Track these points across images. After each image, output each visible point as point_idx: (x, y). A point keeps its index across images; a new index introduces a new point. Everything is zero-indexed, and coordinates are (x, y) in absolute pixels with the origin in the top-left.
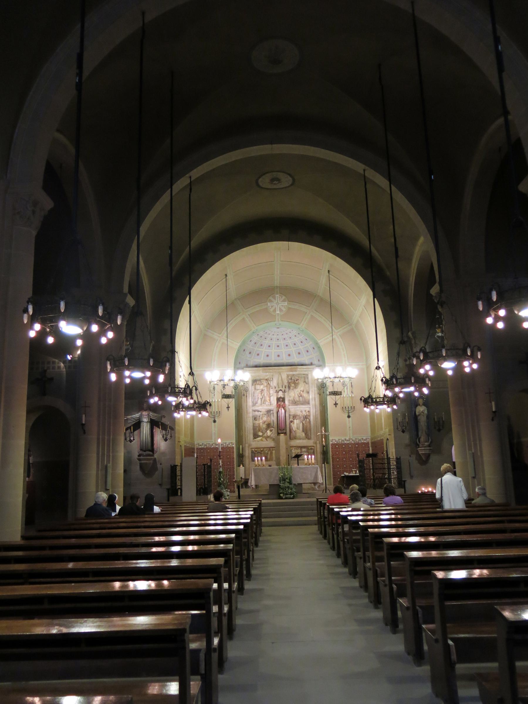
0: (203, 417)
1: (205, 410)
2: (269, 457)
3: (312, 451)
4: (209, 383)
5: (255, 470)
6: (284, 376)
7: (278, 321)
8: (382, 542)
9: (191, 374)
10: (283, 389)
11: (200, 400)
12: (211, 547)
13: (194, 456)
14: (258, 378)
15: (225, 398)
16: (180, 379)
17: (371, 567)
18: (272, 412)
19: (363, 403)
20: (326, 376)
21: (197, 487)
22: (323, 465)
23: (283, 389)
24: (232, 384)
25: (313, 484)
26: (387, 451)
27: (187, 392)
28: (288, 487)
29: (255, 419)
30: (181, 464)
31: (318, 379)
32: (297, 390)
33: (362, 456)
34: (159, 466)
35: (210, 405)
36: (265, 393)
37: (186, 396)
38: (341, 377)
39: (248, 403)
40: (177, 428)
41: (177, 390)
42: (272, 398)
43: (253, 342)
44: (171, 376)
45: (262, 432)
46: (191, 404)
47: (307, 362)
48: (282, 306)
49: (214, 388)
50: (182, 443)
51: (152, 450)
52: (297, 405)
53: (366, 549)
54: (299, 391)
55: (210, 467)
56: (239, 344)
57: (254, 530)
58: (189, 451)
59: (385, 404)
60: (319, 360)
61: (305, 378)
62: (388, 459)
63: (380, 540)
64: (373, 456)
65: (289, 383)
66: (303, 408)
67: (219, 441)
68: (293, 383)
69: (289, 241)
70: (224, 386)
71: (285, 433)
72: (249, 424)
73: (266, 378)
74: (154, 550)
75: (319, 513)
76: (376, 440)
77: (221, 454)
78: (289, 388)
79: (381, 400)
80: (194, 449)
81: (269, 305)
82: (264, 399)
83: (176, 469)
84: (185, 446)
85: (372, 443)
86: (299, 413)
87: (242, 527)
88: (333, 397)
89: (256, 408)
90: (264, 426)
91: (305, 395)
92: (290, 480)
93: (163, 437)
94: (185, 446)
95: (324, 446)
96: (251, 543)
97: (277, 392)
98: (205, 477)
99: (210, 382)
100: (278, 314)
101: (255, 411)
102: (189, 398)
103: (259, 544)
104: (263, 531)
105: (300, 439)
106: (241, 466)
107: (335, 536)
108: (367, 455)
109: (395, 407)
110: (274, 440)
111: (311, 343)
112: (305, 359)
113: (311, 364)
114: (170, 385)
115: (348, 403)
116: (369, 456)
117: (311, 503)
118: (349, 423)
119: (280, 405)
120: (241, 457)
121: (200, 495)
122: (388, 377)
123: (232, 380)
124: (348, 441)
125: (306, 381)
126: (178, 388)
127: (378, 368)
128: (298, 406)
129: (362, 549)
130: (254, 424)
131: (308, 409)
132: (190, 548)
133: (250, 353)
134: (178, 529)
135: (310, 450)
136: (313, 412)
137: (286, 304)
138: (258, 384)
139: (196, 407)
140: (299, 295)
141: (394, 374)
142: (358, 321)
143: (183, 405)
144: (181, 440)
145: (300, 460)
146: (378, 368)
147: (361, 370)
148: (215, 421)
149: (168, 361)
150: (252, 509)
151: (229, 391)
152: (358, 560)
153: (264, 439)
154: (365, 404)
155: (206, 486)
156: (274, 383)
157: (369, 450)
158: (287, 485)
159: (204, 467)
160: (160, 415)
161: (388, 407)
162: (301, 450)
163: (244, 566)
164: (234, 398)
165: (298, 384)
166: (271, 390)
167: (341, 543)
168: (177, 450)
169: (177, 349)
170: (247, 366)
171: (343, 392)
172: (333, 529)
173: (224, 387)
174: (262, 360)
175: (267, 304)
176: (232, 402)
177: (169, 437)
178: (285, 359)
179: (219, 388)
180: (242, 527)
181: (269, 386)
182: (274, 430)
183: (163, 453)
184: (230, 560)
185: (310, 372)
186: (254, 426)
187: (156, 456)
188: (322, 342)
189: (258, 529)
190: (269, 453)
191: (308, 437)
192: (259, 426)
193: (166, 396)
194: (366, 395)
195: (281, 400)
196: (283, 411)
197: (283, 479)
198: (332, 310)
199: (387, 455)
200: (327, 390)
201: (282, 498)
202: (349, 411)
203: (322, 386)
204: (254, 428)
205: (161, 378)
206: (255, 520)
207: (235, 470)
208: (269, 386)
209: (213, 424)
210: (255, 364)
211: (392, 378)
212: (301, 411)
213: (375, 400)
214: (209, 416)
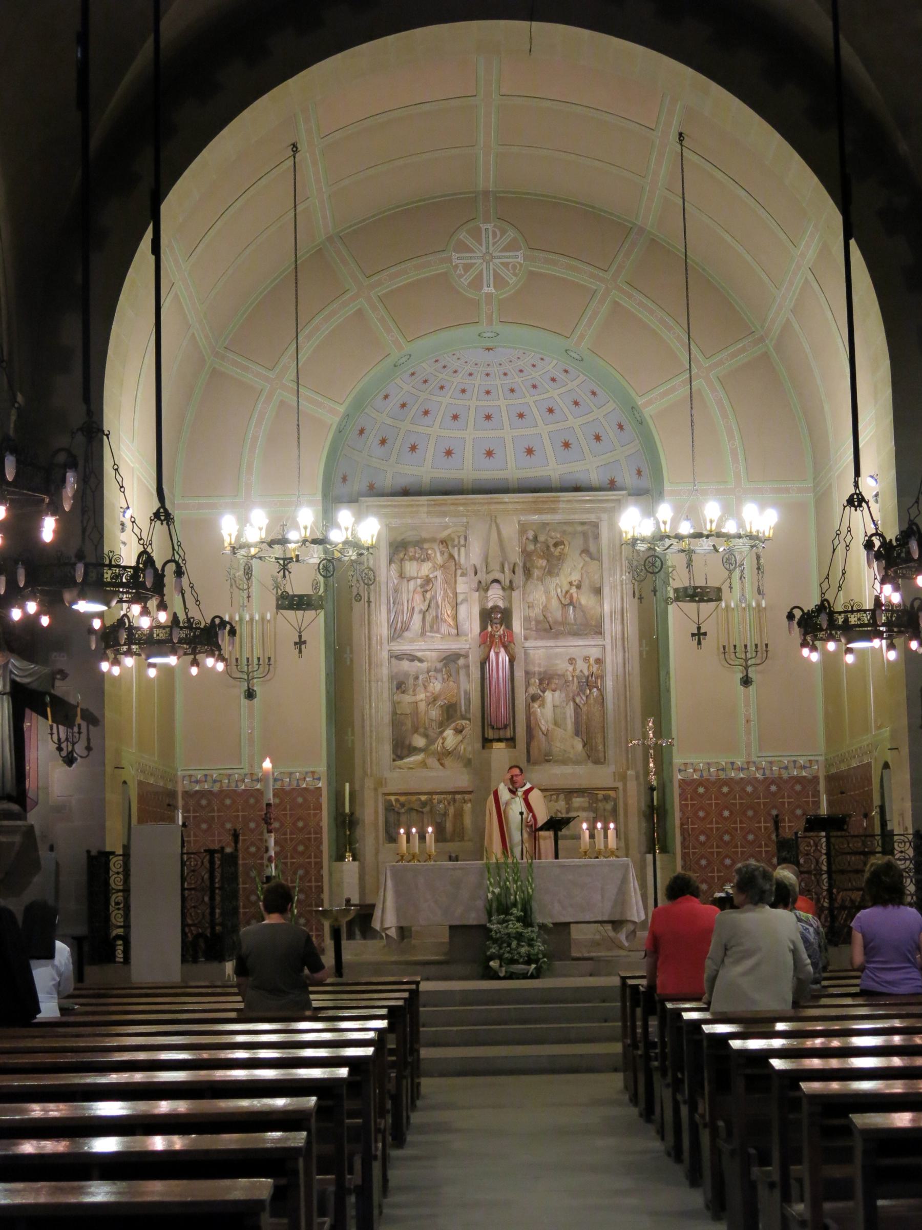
0: (206, 673)
1: (214, 649)
2: (449, 826)
3: (609, 806)
4: (228, 550)
5: (398, 876)
6: (510, 529)
7: (490, 322)
8: (848, 1130)
9: (163, 515)
10: (505, 578)
11: (194, 613)
12: (230, 1141)
13: (172, 820)
14: (410, 535)
15: (291, 607)
16: (123, 537)
17: (808, 1216)
18: (461, 662)
19: (796, 630)
20: (666, 529)
21: (184, 934)
22: (650, 857)
23: (505, 578)
24: (315, 556)
25: (609, 927)
26: (882, 808)
27: (146, 580)
28: (519, 937)
29: (400, 686)
30: (127, 848)
31: (634, 541)
32: (556, 580)
33: (792, 827)
34: (43, 853)
35: (233, 632)
36: (439, 591)
37: (139, 598)
38: (719, 535)
39: (374, 630)
40: (109, 715)
41: (108, 575)
42: (463, 610)
43: (394, 401)
44: (89, 516)
45: (426, 736)
46: (160, 626)
47: (595, 477)
48: (506, 265)
49: (248, 572)
50: (131, 774)
51: (20, 796)
52: (556, 636)
53: (790, 1157)
54: (566, 587)
55: (231, 860)
56: (342, 409)
57: (391, 1086)
58: (157, 803)
59: (879, 635)
60: (639, 473)
61: (589, 536)
62: (887, 837)
63: (842, 1121)
64: (833, 824)
65: (527, 555)
66: (580, 648)
67: (267, 764)
68: (541, 555)
69: (531, 17)
70: (285, 563)
71: (511, 741)
72: (376, 706)
73: (444, 534)
74: (28, 1147)
75: (628, 1031)
76: (843, 767)
77: (274, 813)
78: (528, 572)
79: (866, 618)
80: (172, 794)
81: (455, 261)
82: (433, 612)
83: (108, 869)
84: (140, 783)
85: (830, 778)
86: (562, 666)
87: (343, 1072)
88: (690, 607)
89: (403, 646)
90: (435, 713)
91: (586, 599)
92: (524, 909)
93: (60, 749)
94: (140, 783)
95: (652, 789)
96: (378, 1130)
97: (482, 588)
98: (212, 898)
99: (234, 549)
100: (489, 295)
101: (399, 657)
102: (153, 603)
103: (409, 1138)
104: (423, 1090)
105: (564, 762)
106: (349, 858)
107: (684, 1110)
108: (808, 821)
109: (914, 645)
110: (468, 763)
111: (611, 406)
112: (589, 469)
113: (612, 486)
114: (80, 556)
115: (744, 632)
116: (815, 824)
117: (600, 994)
118: (747, 704)
119: (492, 636)
120: (347, 825)
121: (195, 961)
122: (892, 534)
123: (315, 542)
124: (742, 769)
125: (592, 549)
126: (110, 566)
127: (856, 501)
128: (560, 643)
129: (776, 1155)
130: (395, 705)
131: (594, 653)
132: (158, 1143)
133: (383, 442)
134: (114, 1078)
135: (601, 803)
136: (613, 663)
137: (519, 257)
138: (413, 559)
139: (181, 641)
140: (568, 227)
141: (912, 523)
142: (787, 326)
143: (132, 630)
144: (124, 763)
145: (566, 837)
146: (856, 501)
147: (793, 514)
148: (250, 695)
149: (73, 465)
150: (384, 1012)
151: (301, 582)
152: (763, 1192)
153: (432, 762)
154: (805, 634)
155: (218, 928)
156: (472, 555)
157: (817, 804)
158: (515, 927)
159: (212, 862)
160: (46, 670)
161: (891, 646)
162: (568, 801)
163: (351, 1212)
164: (321, 607)
165: (561, 558)
166: (460, 579)
167: (705, 1138)
168: (113, 798)
169: (109, 421)
170: (374, 491)
171: (725, 589)
172: (677, 1085)
173: (284, 568)
174: (427, 468)
175: (450, 260)
176: (315, 624)
177: (80, 749)
178: (512, 467)
179: (265, 571)
180: (343, 1072)
181: (452, 566)
182: (472, 728)
183: (60, 810)
184: (298, 1186)
185: (604, 516)
186: (394, 713)
187: (33, 818)
188: (652, 406)
189: (406, 1083)
190: (451, 811)
191: (594, 754)
192: (416, 713)
193: (67, 596)
194: (811, 603)
195: (495, 619)
196: (504, 657)
197: (501, 907)
198: (696, 291)
199: (884, 824)
200: (667, 583)
201: (495, 976)
202: (747, 661)
203: (648, 566)
204: (397, 721)
205: (48, 529)
206: (392, 1052)
207: (325, 872)
208: (452, 566)
209: (245, 702)
210: (403, 482)
211: (905, 536)
212: (572, 661)
213: (840, 619)
214: (227, 671)
